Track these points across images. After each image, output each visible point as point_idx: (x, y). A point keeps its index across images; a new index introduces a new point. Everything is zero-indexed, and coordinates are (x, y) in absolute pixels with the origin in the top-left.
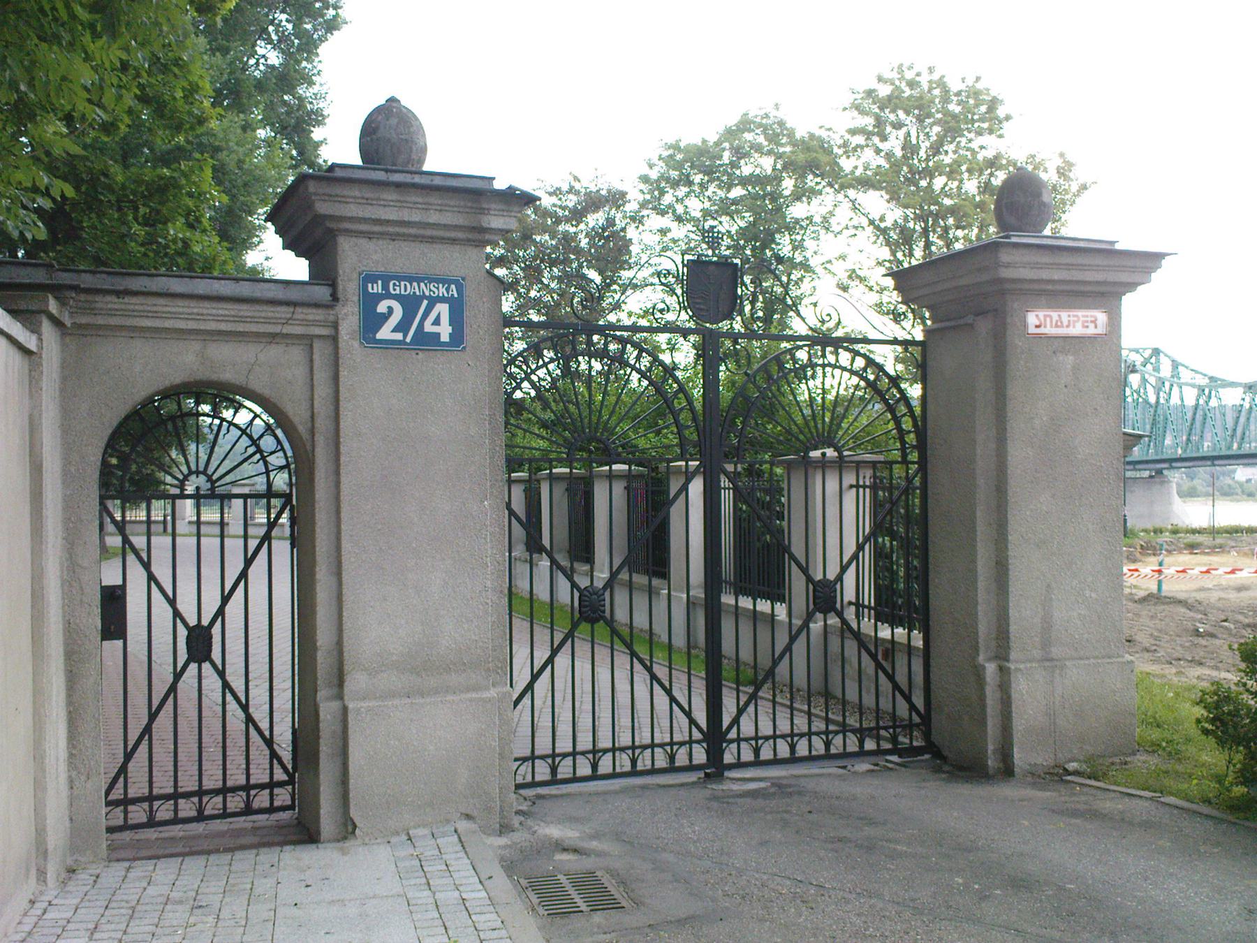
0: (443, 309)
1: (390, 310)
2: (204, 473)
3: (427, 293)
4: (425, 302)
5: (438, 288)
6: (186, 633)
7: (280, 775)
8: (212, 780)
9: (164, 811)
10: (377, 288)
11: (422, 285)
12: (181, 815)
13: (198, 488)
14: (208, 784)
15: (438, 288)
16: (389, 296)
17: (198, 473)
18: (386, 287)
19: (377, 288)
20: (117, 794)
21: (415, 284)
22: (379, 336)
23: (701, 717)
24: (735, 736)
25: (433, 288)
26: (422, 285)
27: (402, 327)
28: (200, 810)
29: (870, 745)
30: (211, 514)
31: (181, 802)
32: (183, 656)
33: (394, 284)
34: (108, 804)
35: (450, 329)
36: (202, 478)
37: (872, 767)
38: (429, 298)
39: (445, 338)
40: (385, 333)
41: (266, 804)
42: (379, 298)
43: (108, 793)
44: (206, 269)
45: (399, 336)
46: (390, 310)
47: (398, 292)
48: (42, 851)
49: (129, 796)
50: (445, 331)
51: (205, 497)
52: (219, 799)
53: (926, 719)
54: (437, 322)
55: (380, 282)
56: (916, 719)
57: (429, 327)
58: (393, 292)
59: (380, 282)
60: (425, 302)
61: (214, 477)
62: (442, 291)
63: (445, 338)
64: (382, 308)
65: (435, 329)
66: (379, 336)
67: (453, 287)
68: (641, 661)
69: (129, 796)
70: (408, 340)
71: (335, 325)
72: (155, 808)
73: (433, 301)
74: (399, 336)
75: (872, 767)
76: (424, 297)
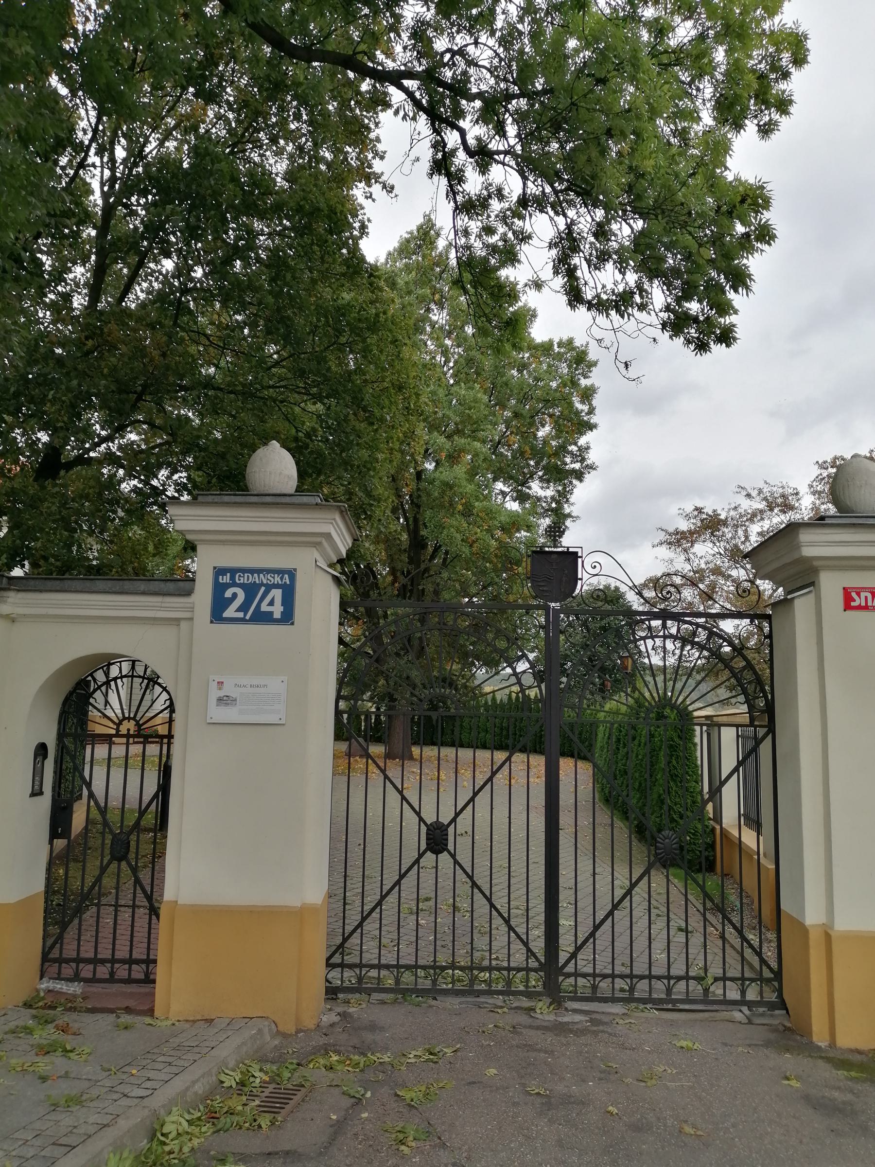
0: (277, 594)
1: (235, 596)
2: (134, 719)
3: (265, 582)
4: (263, 589)
5: (274, 578)
6: (426, 828)
7: (533, 963)
8: (122, 953)
9: (122, 972)
10: (226, 579)
11: (261, 575)
12: (98, 976)
13: (129, 730)
14: (119, 955)
15: (274, 578)
16: (234, 584)
17: (129, 719)
18: (232, 578)
19: (226, 579)
20: (337, 959)
21: (256, 575)
22: (225, 615)
23: (538, 945)
24: (573, 970)
25: (269, 578)
26: (261, 575)
27: (244, 608)
28: (112, 973)
29: (752, 994)
30: (136, 749)
31: (134, 967)
32: (423, 846)
33: (240, 576)
34: (328, 965)
35: (282, 609)
36: (133, 722)
37: (626, 1011)
38: (266, 585)
39: (277, 615)
40: (230, 612)
41: (90, 975)
42: (227, 586)
43: (328, 959)
44: (107, 574)
45: (240, 615)
46: (235, 596)
47: (242, 581)
48: (332, 999)
49: (134, 957)
50: (277, 610)
51: (133, 736)
52: (91, 967)
53: (778, 975)
54: (271, 603)
55: (228, 574)
56: (767, 974)
57: (264, 608)
58: (238, 581)
59: (228, 574)
60: (263, 589)
61: (141, 722)
62: (277, 579)
63: (277, 615)
64: (228, 594)
65: (270, 609)
66: (225, 615)
67: (286, 576)
68: (144, 891)
69: (134, 957)
70: (248, 617)
71: (192, 609)
72: (80, 968)
73: (269, 588)
74: (240, 615)
75: (626, 1011)
76: (262, 584)
